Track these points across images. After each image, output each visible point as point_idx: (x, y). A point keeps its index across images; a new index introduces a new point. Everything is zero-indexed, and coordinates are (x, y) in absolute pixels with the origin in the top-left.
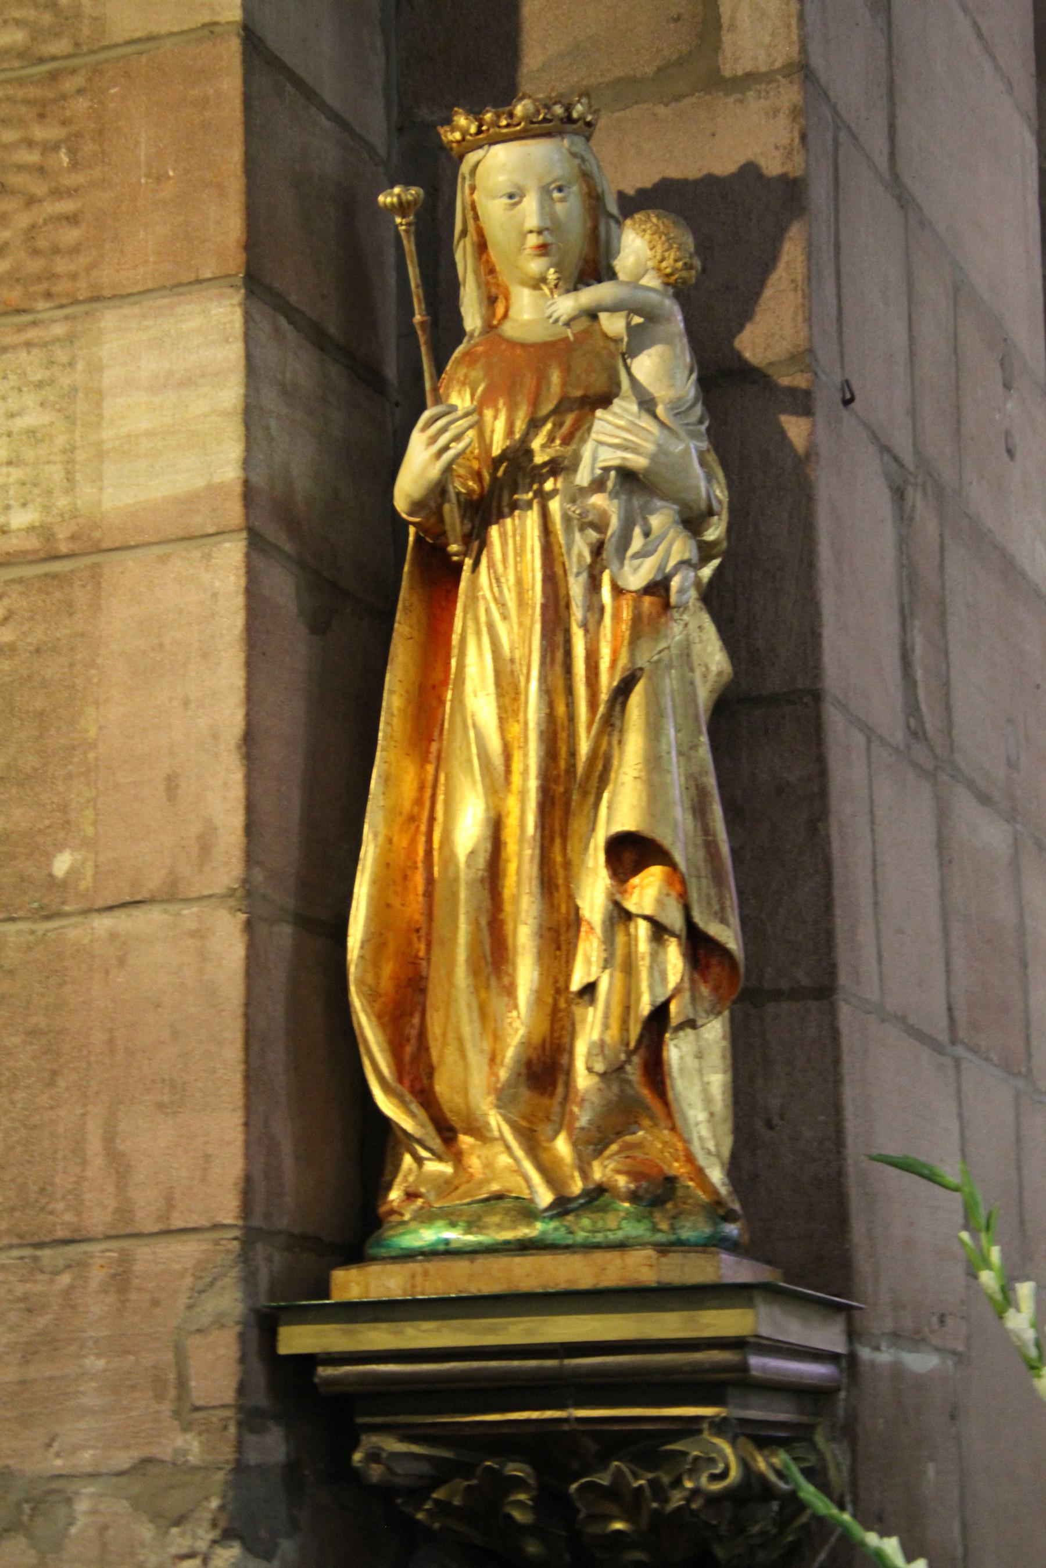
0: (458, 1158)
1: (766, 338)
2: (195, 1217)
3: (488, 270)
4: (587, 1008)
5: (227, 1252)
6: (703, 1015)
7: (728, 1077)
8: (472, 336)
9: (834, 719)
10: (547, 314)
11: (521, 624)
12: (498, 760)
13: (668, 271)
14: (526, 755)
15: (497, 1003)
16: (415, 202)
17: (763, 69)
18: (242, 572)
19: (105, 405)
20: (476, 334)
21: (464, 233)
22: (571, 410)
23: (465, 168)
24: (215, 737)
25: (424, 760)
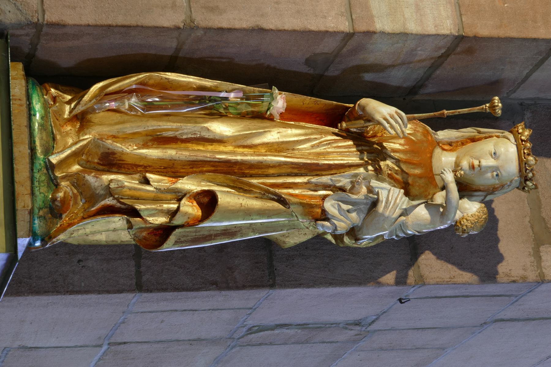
1: (429, 264)
2: (48, 2)
4: (138, 180)
5: (32, 16)
6: (134, 233)
8: (435, 134)
9: (262, 293)
10: (445, 169)
11: (310, 154)
12: (249, 142)
13: (462, 223)
14: (251, 155)
16: (495, 113)
17: (543, 264)
18: (335, 30)
20: (436, 136)
21: (479, 132)
22: (403, 178)
23: (507, 133)
24: (262, 15)
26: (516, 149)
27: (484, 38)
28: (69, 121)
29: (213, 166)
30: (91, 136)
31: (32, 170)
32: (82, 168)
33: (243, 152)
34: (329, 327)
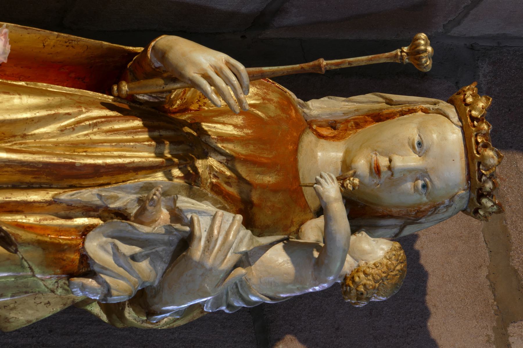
8: (303, 106)
11: (57, 145)
13: (357, 279)
20: (305, 110)
21: (390, 102)
23: (443, 105)
26: (460, 135)
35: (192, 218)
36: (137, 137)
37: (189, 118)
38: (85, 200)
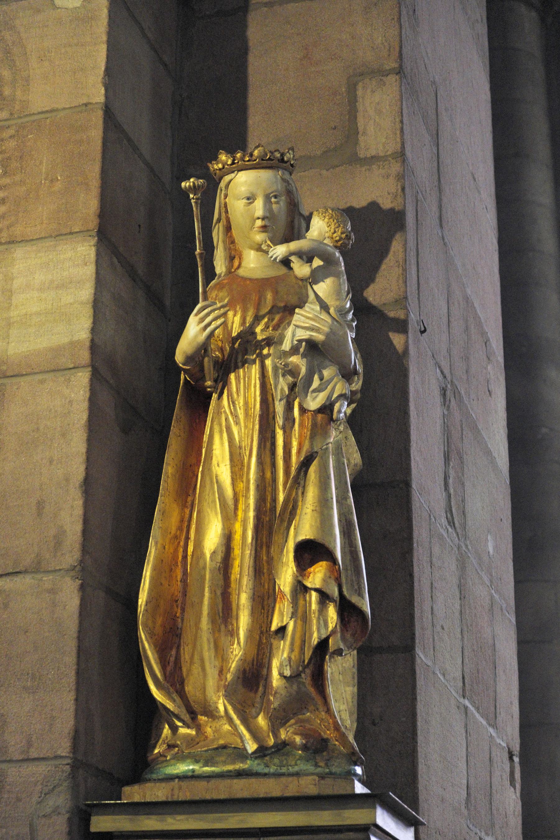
0: (199, 728)
1: (376, 294)
3: (230, 242)
4: (280, 641)
5: (63, 771)
7: (355, 690)
8: (220, 276)
11: (246, 427)
12: (230, 502)
13: (338, 238)
15: (224, 640)
17: (382, 154)
18: (88, 389)
19: (13, 297)
20: (222, 275)
21: (219, 220)
22: (278, 313)
23: (222, 184)
24: (67, 480)
25: (184, 506)
26: (242, 172)
27: (101, 205)
28: (200, 729)
29: (261, 547)
30: (221, 701)
31: (265, 775)
32: (262, 713)
33: (243, 511)
34: (447, 427)
35: (297, 341)
36: (242, 377)
37: (229, 345)
38: (283, 409)
